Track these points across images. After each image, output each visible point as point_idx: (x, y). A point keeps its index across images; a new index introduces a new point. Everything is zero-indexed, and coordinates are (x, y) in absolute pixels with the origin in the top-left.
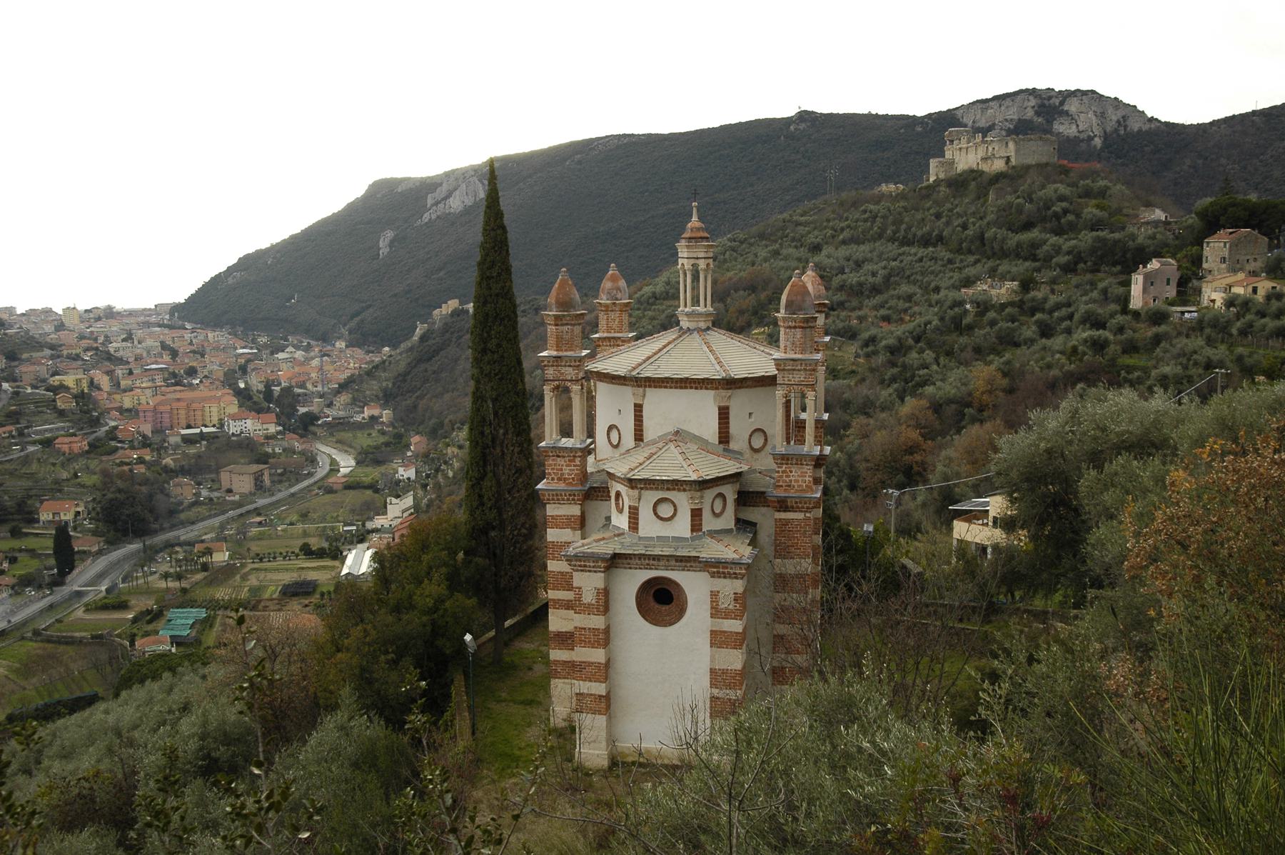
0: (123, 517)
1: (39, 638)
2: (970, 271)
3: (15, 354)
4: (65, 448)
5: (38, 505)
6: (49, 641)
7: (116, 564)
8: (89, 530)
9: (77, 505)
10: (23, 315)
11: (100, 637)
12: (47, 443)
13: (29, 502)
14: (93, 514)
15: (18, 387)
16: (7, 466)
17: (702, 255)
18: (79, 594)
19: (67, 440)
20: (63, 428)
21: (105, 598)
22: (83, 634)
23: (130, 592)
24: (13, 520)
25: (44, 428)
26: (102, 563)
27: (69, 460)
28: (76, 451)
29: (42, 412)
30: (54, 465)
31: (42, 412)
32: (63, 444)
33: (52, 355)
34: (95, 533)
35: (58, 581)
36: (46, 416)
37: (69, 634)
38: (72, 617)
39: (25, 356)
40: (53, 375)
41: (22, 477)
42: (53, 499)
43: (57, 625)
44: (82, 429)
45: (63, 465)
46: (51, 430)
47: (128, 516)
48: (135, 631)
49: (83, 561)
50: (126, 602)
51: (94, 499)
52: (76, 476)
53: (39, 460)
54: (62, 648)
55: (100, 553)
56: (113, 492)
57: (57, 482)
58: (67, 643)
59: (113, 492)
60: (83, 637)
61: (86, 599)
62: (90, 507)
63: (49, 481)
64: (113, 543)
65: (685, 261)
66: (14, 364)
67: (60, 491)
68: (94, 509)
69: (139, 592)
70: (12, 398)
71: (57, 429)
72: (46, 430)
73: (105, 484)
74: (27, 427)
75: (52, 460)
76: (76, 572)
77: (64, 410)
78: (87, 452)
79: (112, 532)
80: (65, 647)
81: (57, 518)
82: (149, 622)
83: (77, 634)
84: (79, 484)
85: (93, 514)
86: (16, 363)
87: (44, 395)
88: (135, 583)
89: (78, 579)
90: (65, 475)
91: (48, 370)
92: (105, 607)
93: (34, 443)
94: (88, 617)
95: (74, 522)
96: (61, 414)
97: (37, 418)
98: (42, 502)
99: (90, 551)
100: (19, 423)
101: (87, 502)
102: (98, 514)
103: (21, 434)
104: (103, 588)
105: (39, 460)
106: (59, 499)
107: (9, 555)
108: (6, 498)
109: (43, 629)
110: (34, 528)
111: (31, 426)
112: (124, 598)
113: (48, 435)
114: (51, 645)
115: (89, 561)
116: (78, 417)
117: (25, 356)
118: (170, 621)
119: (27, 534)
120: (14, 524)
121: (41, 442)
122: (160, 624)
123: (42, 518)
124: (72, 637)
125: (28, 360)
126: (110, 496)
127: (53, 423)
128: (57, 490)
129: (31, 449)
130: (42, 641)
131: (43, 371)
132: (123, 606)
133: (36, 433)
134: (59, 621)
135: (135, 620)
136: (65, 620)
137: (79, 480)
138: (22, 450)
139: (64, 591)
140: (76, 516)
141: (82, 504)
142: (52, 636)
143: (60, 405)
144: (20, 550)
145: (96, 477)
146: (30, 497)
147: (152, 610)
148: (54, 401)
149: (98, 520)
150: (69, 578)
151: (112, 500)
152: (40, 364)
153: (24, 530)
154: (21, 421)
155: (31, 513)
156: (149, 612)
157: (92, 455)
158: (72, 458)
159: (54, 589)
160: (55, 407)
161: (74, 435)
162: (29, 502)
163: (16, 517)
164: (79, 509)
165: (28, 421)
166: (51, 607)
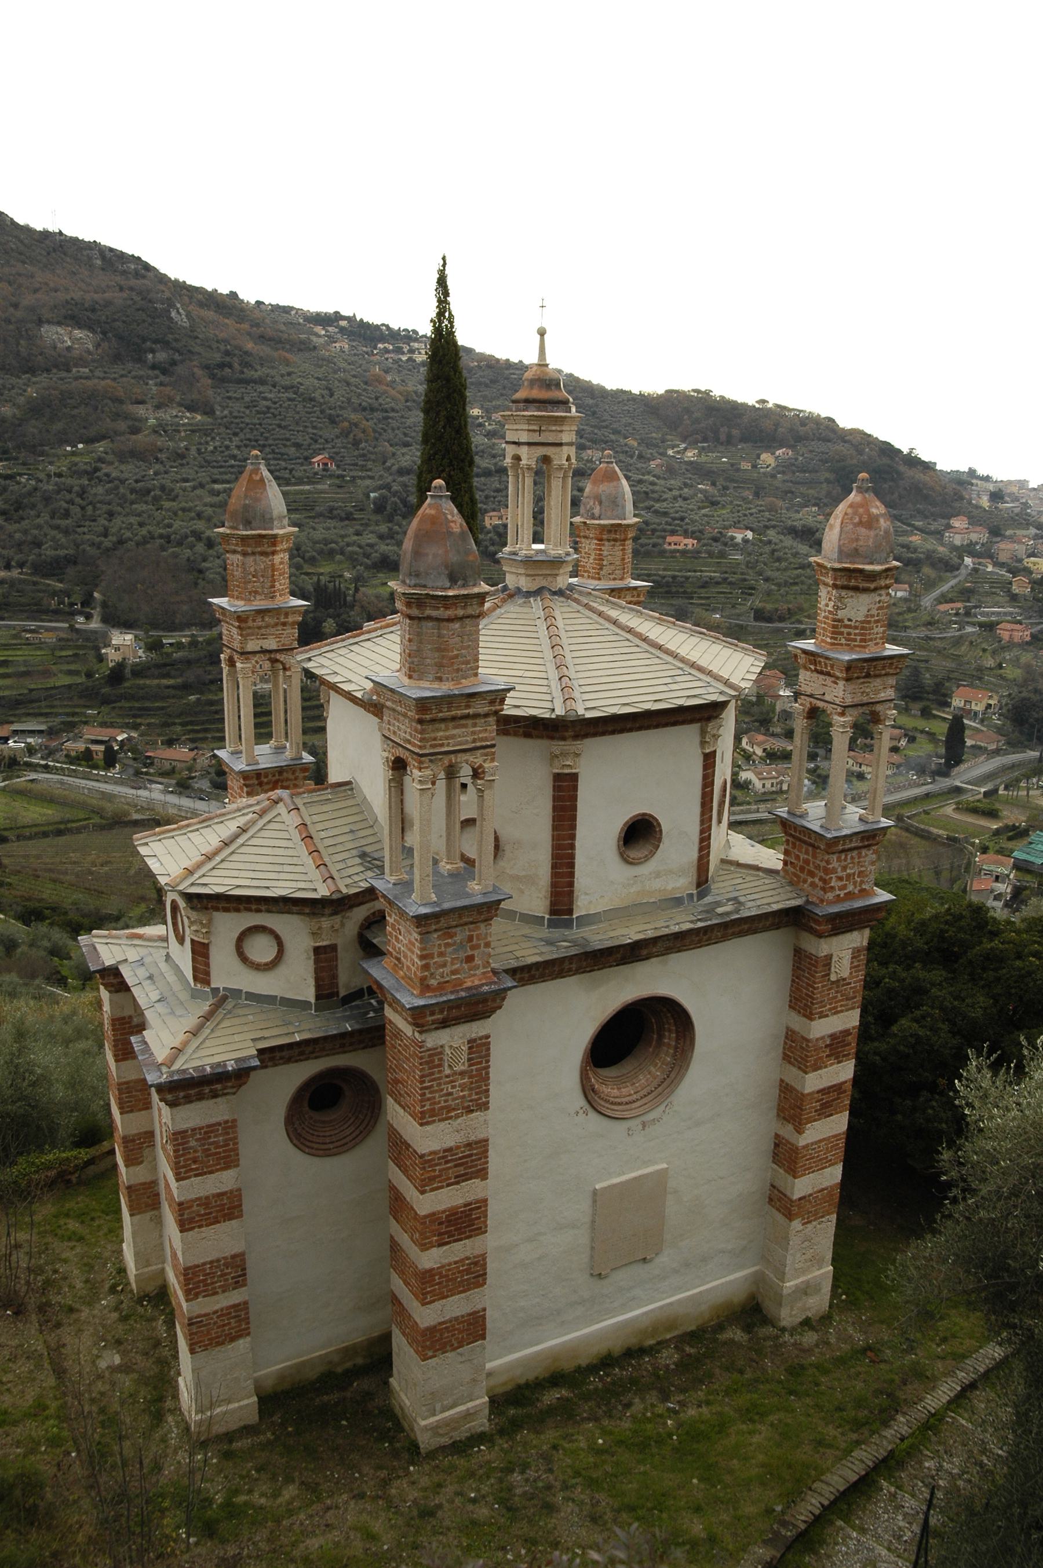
0: (1031, 720)
1: (900, 824)
2: (810, 1338)
3: (999, 529)
4: (1005, 636)
5: (954, 689)
6: (907, 830)
7: (1009, 768)
8: (996, 726)
9: (991, 697)
10: (1034, 489)
11: (954, 840)
12: (989, 627)
13: (947, 684)
14: (1004, 711)
15: (980, 564)
16: (938, 644)
17: (524, 437)
18: (958, 790)
19: (1009, 626)
20: (1011, 614)
21: (978, 801)
22: (941, 832)
23: (1007, 802)
24: (928, 700)
25: (990, 611)
26: (997, 762)
27: (1002, 648)
28: (1016, 640)
29: (994, 593)
30: (984, 650)
31: (994, 593)
32: (1004, 632)
33: (1036, 535)
34: (999, 731)
35: (944, 772)
36: (997, 598)
37: (927, 828)
38: (941, 811)
39: (1008, 533)
40: (1029, 556)
41: (948, 657)
42: (971, 686)
43: (923, 816)
44: (1030, 618)
45: (994, 653)
46: (999, 613)
47: (1037, 720)
48: (991, 844)
49: (976, 756)
50: (997, 811)
51: (1010, 695)
52: (1000, 666)
53: (971, 643)
54: (915, 841)
55: (997, 752)
56: (1029, 691)
57: (980, 669)
58: (922, 837)
59: (1029, 691)
60: (939, 836)
61: (963, 797)
62: (1004, 702)
63: (973, 666)
64: (1014, 745)
65: (523, 451)
66: (994, 540)
67: (980, 679)
68: (1007, 704)
69: (1014, 803)
70: (970, 574)
71: (1005, 614)
72: (993, 613)
73: (1025, 681)
74: (976, 607)
75: (985, 646)
76: (963, 767)
77: (1016, 595)
78: (1027, 643)
79: (1016, 734)
80: (919, 839)
81: (968, 707)
82: (1010, 839)
83: (935, 831)
84: (1000, 675)
85: (1004, 711)
86: (999, 539)
87: (1002, 575)
88: (1015, 793)
89: (961, 777)
90: (990, 663)
91: (1027, 550)
92: (974, 811)
93: (973, 624)
94: (957, 816)
95: (984, 714)
96: (1014, 598)
97: (988, 599)
98: (958, 687)
99: (986, 748)
100: (969, 601)
101: (1002, 696)
102: (1008, 711)
103: (967, 614)
104: (983, 790)
105: (971, 643)
106: (977, 687)
107: (910, 734)
108: (928, 676)
109: (908, 817)
110: (944, 712)
111: (980, 607)
112: (997, 806)
113: (993, 619)
114: (907, 834)
115: (982, 758)
116: (1030, 604)
117: (1008, 533)
118: (1031, 843)
119: (935, 717)
120: (928, 703)
121: (981, 625)
122: (1021, 843)
123: (954, 703)
124: (929, 832)
125: (1011, 537)
126: (1023, 695)
127: (1002, 607)
128: (977, 677)
129: (969, 629)
130: (901, 828)
131: (1021, 550)
132: (992, 814)
133: (983, 614)
134: (926, 813)
135: (997, 833)
136: (933, 813)
137: (1002, 671)
138: (960, 630)
139: (944, 783)
140: (987, 708)
141: (996, 697)
142: (912, 826)
143: (1015, 589)
144: (922, 732)
145: (1019, 671)
146: (949, 679)
147: (1018, 827)
148: (1010, 583)
149: (1006, 718)
150: (956, 770)
151: (1024, 699)
152: (1020, 542)
153: (935, 712)
154: (972, 600)
155: (945, 695)
156: (1014, 827)
157: (1031, 648)
158: (1011, 645)
159: (937, 778)
160: (1009, 591)
161: (1020, 623)
162: (947, 684)
163: (931, 696)
164: (991, 702)
165: (980, 601)
166: (927, 796)
